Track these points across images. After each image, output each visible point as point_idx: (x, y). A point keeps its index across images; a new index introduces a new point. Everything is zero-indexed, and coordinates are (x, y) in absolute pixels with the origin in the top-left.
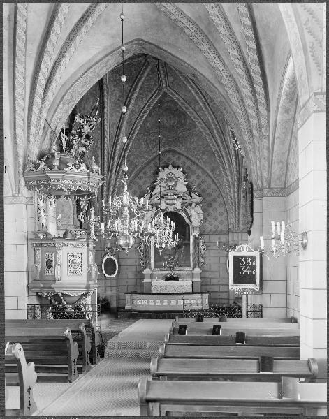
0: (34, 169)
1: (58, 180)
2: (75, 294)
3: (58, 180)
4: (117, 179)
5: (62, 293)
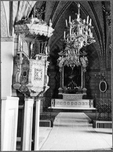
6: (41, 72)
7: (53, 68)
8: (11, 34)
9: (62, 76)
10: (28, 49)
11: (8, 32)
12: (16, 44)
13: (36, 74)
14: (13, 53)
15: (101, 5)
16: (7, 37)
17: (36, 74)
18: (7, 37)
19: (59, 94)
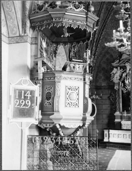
0: (39, 11)
1: (60, 18)
2: (72, 126)
3: (60, 18)
4: (96, 50)
5: (59, 125)
6: (77, 91)
7: (105, 85)
8: (24, 32)
9: (119, 96)
10: (66, 59)
11: (19, 28)
12: (34, 46)
13: (68, 96)
14: (29, 64)
15: (91, 169)
16: (18, 35)
17: (68, 97)
18: (18, 36)
19: (116, 120)
